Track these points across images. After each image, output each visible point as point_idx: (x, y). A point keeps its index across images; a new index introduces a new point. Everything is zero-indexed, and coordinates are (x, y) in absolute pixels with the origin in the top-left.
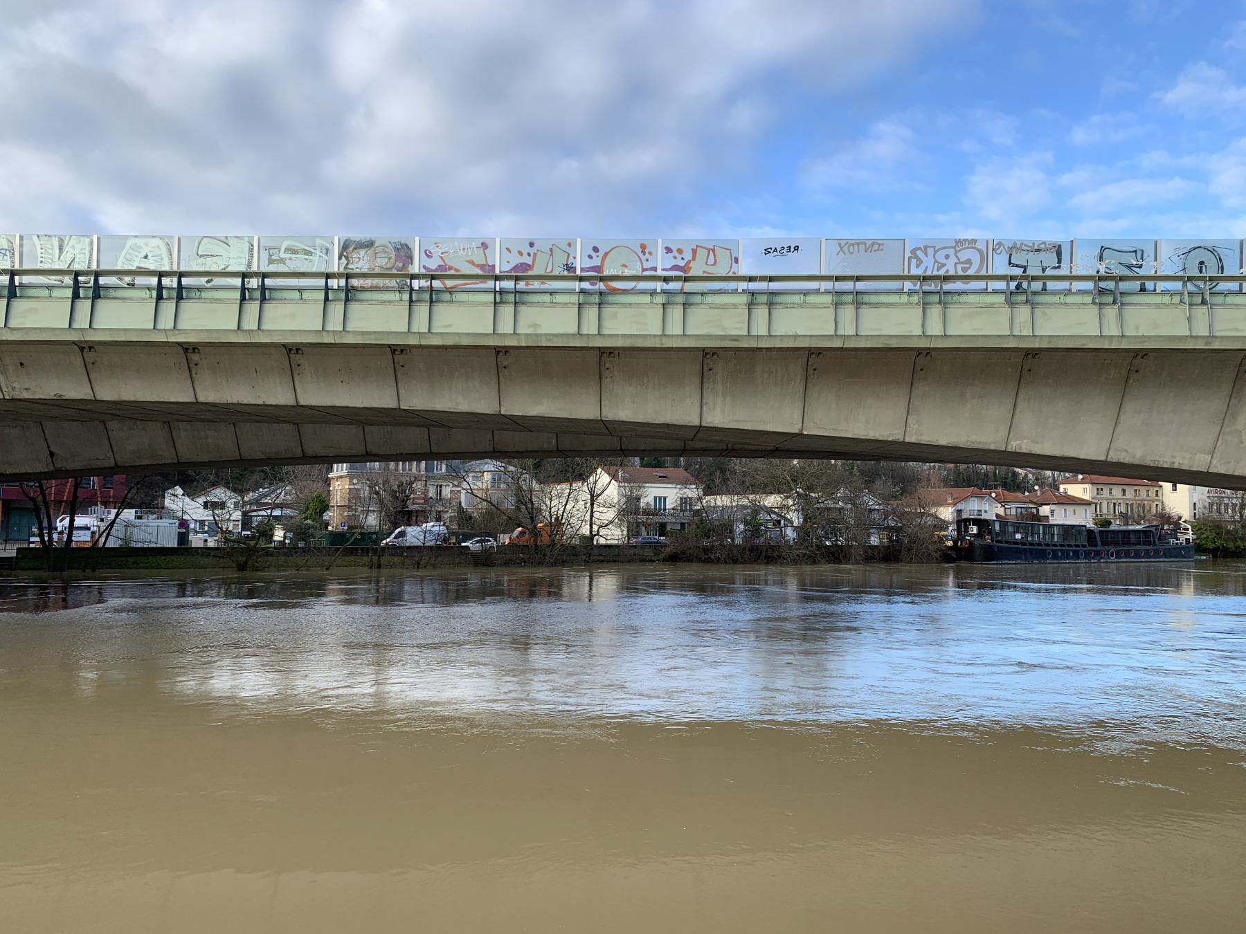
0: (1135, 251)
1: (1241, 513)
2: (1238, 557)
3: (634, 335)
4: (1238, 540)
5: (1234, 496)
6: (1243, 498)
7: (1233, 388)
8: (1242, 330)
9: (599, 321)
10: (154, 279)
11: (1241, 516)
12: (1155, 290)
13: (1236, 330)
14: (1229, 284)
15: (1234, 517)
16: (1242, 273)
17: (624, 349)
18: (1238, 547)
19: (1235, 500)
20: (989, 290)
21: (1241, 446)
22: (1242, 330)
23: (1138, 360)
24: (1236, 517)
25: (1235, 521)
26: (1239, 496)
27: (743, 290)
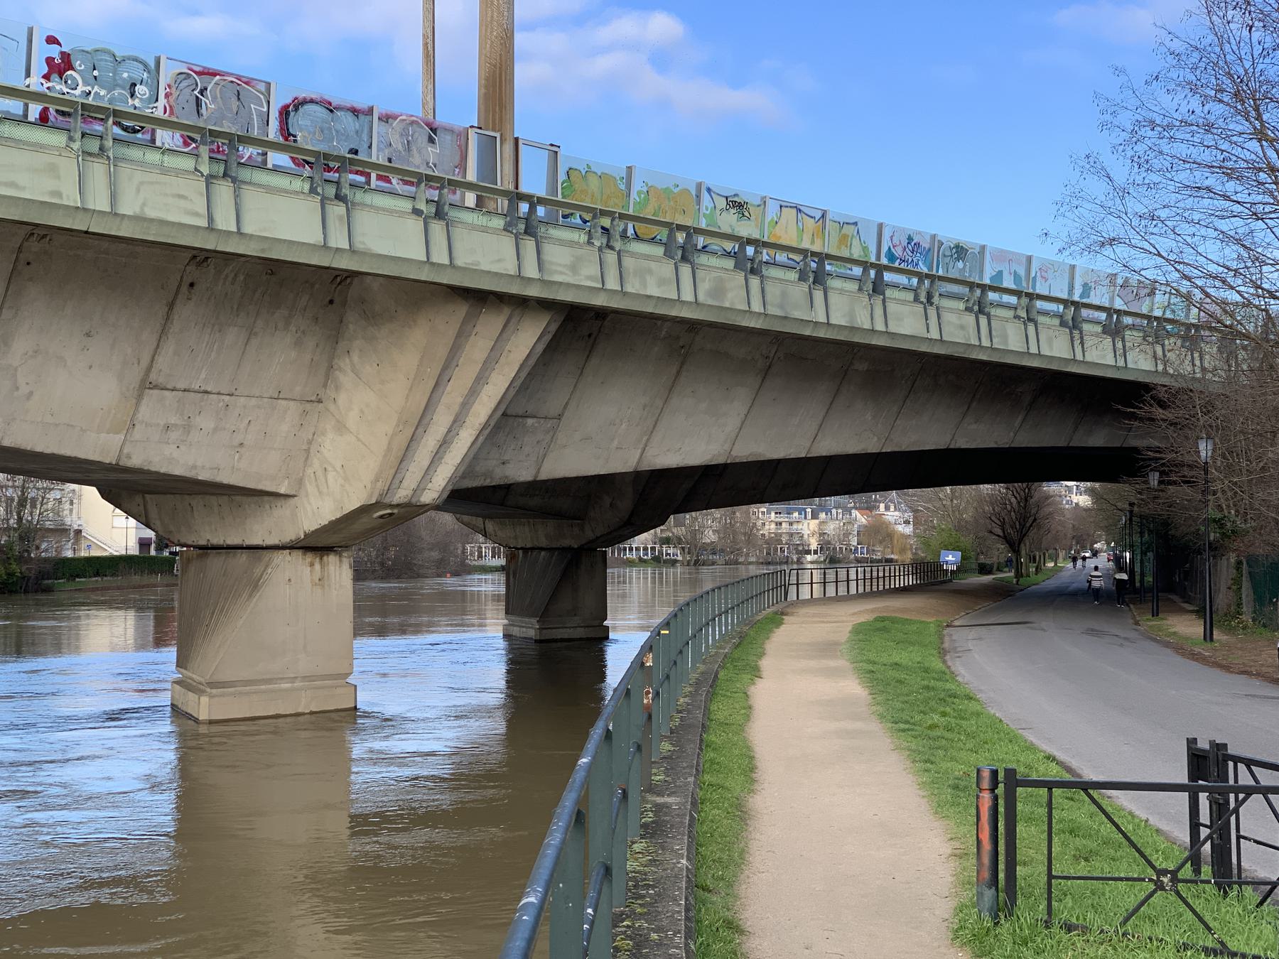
0: (781, 207)
1: (18, 514)
2: (11, 592)
3: (669, 299)
4: (12, 561)
5: (10, 483)
6: (23, 487)
7: (7, 291)
8: (24, 188)
9: (518, 259)
10: (1107, 302)
11: (20, 519)
12: (26, 115)
13: (13, 185)
14: (7, 101)
15: (8, 520)
16: (28, 86)
17: (712, 325)
18: (10, 575)
19: (11, 490)
20: (270, 166)
21: (16, 393)
22: (24, 188)
23: (34, 245)
24: (12, 521)
25: (9, 529)
26: (17, 484)
27: (273, 165)
